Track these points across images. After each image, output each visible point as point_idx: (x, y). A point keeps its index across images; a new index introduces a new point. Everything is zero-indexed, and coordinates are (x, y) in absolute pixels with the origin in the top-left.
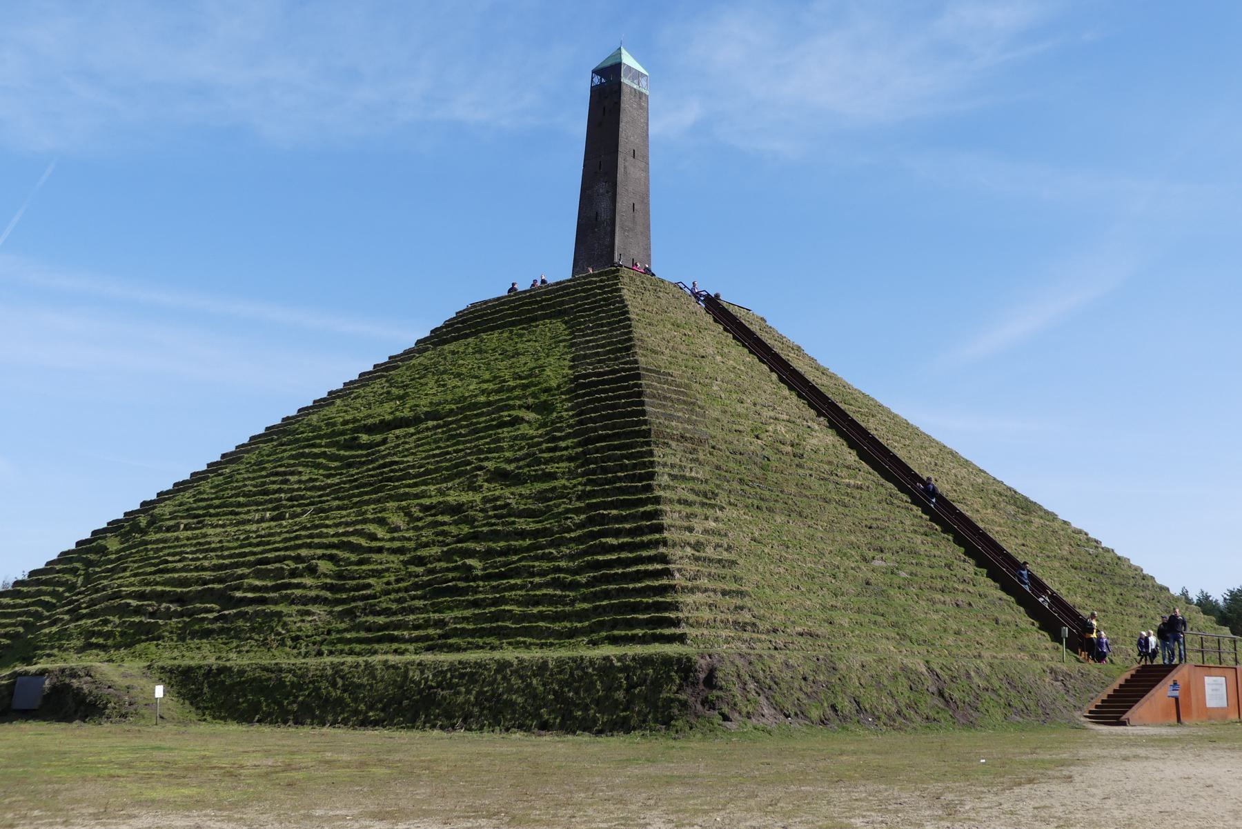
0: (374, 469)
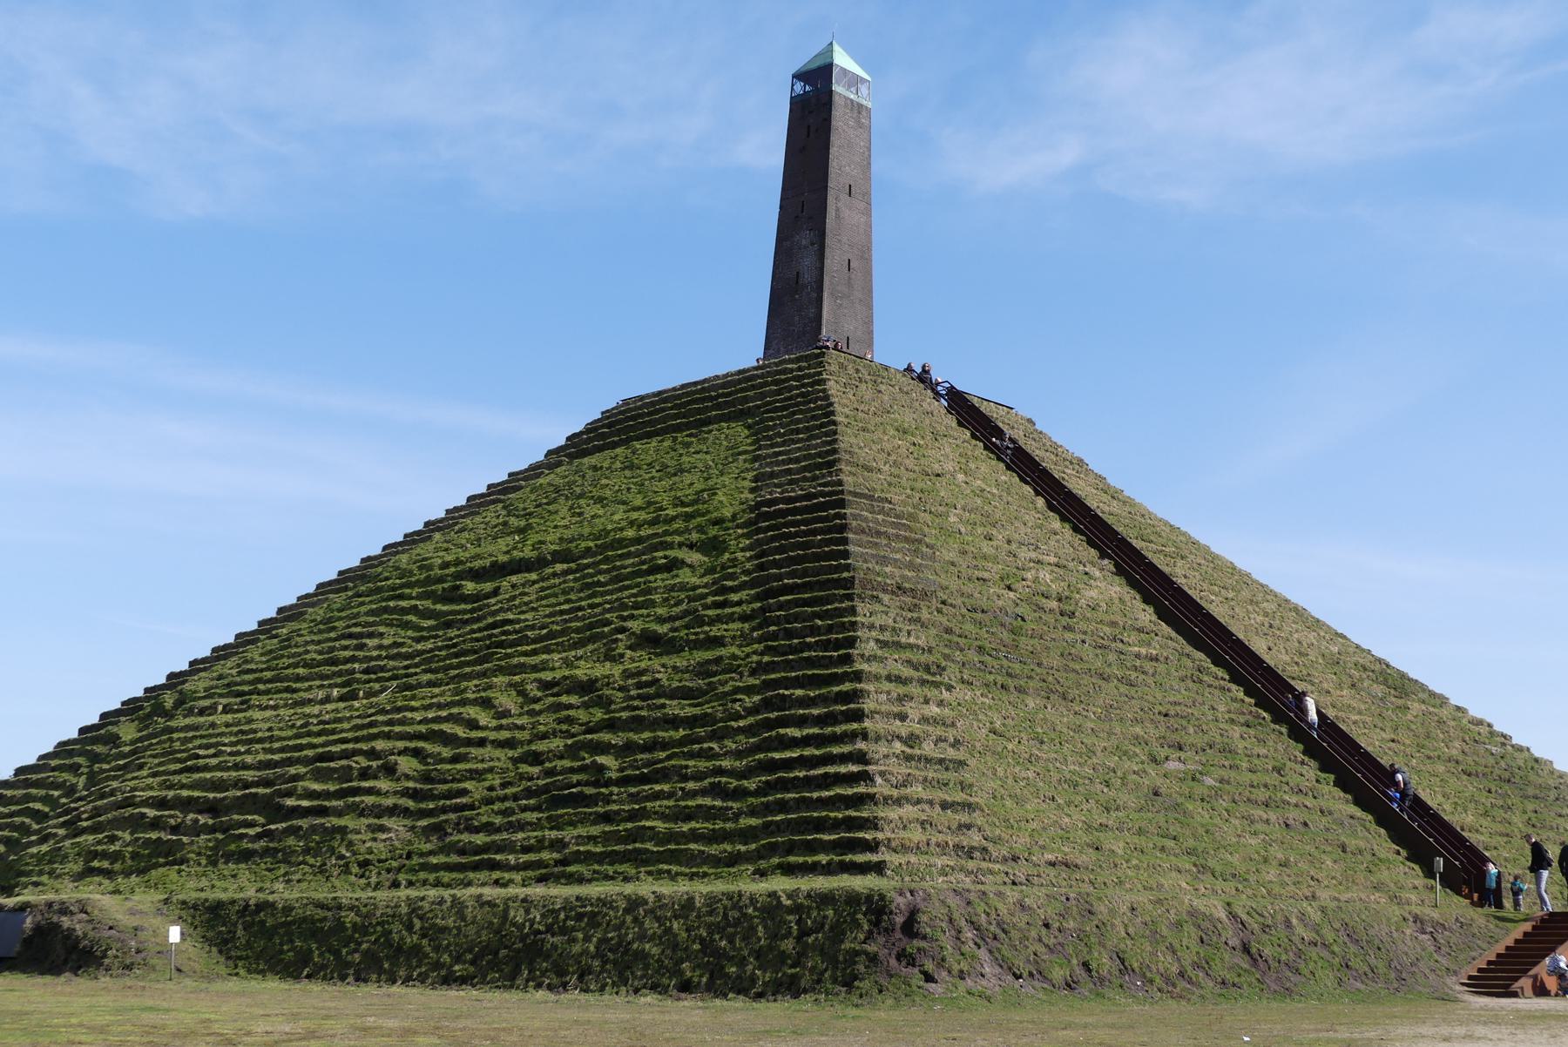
0: (480, 630)
